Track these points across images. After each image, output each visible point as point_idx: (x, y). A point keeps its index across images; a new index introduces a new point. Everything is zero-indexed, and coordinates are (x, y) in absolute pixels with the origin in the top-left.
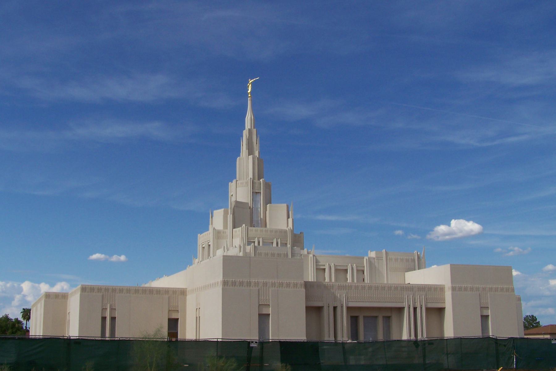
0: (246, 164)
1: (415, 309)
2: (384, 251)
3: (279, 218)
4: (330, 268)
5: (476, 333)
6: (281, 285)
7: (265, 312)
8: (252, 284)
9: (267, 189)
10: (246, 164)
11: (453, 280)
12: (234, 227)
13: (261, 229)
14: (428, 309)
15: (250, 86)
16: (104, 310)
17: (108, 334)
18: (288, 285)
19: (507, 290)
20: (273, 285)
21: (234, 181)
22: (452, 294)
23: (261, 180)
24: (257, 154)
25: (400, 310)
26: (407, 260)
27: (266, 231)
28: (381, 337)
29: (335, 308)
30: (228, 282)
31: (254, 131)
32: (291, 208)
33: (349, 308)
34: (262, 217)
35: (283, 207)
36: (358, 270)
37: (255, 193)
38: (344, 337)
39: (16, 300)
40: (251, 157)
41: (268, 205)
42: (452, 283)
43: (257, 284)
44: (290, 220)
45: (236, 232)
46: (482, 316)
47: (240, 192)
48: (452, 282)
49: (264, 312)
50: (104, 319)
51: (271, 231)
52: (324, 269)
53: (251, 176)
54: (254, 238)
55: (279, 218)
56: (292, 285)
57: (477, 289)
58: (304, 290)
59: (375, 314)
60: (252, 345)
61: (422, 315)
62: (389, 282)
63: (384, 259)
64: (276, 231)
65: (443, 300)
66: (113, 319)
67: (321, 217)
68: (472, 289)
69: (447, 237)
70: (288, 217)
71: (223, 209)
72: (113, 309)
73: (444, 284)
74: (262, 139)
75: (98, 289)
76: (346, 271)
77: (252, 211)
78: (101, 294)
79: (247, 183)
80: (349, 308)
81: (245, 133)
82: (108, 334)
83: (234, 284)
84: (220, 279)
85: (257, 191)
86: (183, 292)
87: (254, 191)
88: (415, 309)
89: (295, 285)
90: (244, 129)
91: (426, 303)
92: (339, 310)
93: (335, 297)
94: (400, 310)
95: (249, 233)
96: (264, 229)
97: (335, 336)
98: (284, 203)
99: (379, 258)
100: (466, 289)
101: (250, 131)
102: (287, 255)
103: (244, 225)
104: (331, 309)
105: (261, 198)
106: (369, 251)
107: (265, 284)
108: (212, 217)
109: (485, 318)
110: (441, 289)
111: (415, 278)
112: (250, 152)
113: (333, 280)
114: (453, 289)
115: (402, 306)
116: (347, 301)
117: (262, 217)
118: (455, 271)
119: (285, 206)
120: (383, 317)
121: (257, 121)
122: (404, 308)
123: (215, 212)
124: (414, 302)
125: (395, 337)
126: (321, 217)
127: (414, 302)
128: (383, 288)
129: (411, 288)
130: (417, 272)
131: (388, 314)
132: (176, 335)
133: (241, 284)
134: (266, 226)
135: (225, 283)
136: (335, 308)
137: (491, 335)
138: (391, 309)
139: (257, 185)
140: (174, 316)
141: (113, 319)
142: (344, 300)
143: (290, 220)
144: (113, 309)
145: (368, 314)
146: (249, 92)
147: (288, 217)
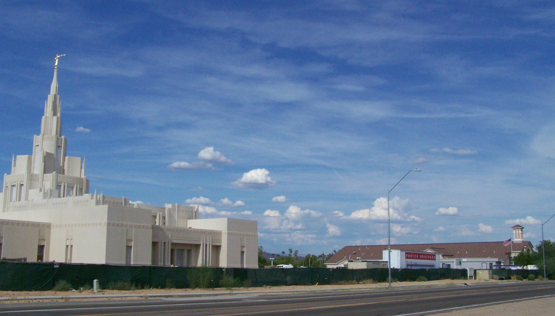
0: (50, 122)
1: (206, 245)
2: (176, 204)
6: (139, 227)
9: (67, 143)
10: (50, 122)
11: (229, 228)
12: (44, 173)
14: (213, 246)
15: (57, 60)
20: (135, 226)
21: (41, 135)
23: (63, 137)
24: (59, 115)
25: (198, 246)
29: (165, 243)
31: (58, 97)
34: (61, 165)
37: (58, 147)
38: (168, 264)
39: (447, 261)
40: (55, 118)
41: (67, 157)
43: (126, 226)
47: (44, 142)
48: (228, 229)
58: (151, 231)
59: (182, 248)
60: (55, 267)
61: (210, 249)
63: (177, 210)
65: (220, 241)
73: (221, 230)
79: (52, 138)
80: (173, 244)
81: (50, 98)
83: (114, 225)
84: (105, 220)
86: (49, 226)
88: (206, 245)
90: (49, 93)
91: (212, 242)
92: (167, 244)
94: (198, 246)
96: (62, 175)
97: (164, 263)
99: (173, 208)
102: (121, 203)
104: (163, 244)
107: (131, 226)
108: (15, 161)
111: (194, 224)
112: (55, 114)
114: (228, 234)
117: (61, 165)
118: (231, 223)
119: (79, 159)
120: (178, 250)
121: (60, 90)
122: (200, 245)
123: (18, 156)
125: (193, 265)
127: (206, 242)
129: (191, 231)
131: (189, 248)
132: (42, 259)
133: (118, 225)
134: (64, 173)
135: (109, 224)
136: (165, 243)
138: (191, 245)
143: (83, 170)
145: (178, 248)
146: (56, 64)
147: (81, 168)
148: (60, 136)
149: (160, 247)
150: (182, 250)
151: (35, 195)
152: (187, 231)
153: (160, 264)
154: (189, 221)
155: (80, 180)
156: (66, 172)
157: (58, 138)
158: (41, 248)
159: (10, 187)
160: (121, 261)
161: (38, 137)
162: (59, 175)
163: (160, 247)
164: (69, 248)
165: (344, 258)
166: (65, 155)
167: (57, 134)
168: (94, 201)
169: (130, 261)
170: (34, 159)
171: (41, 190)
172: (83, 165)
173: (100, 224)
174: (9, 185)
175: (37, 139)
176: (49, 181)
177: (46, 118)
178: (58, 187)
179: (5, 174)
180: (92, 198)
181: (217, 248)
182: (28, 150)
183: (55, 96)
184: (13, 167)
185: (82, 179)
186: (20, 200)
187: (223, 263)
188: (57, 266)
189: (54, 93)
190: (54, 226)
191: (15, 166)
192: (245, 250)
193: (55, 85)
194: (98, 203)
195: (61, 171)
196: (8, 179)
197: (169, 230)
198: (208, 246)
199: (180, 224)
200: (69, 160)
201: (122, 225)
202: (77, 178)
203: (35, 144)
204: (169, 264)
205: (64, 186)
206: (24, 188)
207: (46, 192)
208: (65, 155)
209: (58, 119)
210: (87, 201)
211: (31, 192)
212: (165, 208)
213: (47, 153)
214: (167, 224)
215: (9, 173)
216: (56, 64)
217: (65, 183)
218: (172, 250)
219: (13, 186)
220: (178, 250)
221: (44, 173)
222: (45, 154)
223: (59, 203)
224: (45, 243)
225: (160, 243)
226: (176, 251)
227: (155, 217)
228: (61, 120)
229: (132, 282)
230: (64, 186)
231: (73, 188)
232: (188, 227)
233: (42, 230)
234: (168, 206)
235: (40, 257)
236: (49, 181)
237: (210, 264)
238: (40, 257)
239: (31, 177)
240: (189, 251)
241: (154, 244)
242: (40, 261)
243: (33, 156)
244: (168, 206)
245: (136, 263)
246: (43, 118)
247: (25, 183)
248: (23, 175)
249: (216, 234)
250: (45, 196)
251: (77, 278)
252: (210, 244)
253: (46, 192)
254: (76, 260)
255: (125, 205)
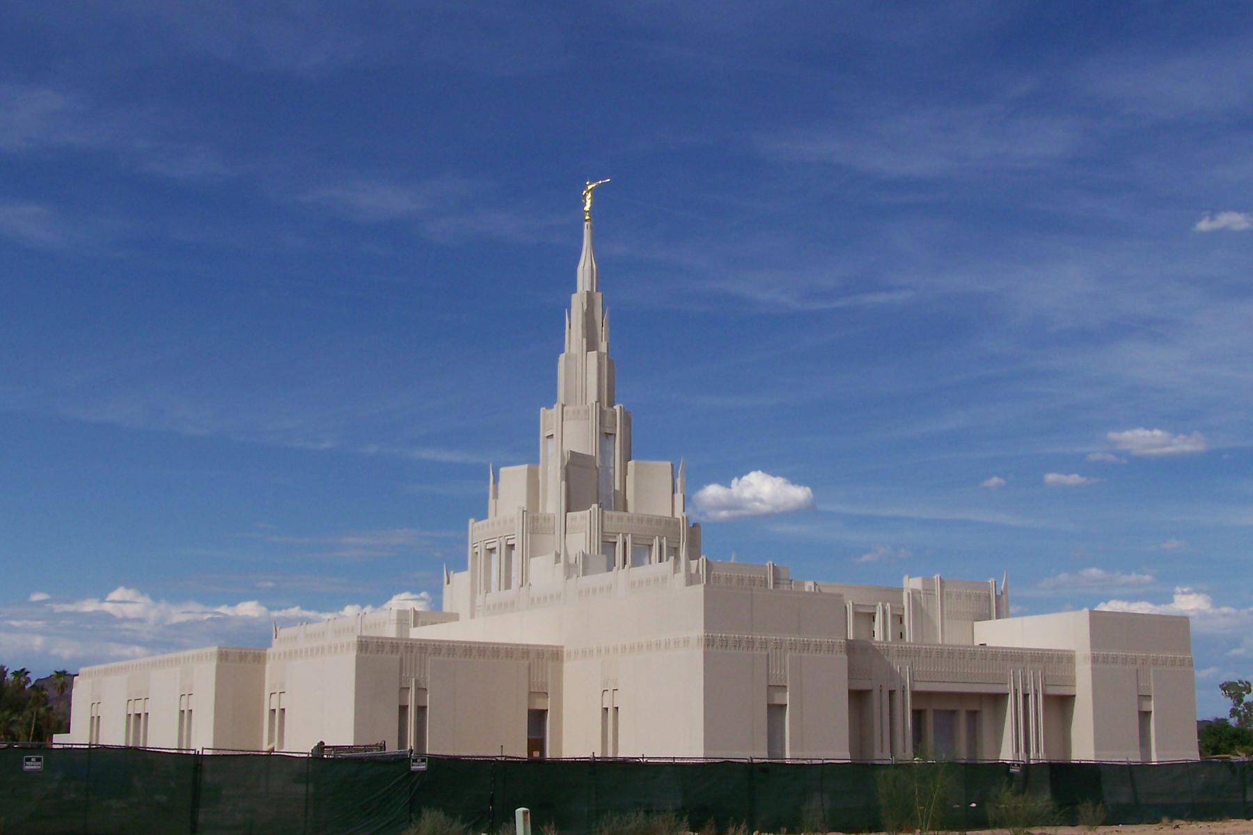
0: (580, 367)
1: (1026, 696)
2: (936, 577)
5: (758, 752)
6: (806, 646)
7: (777, 700)
8: (757, 645)
10: (580, 367)
12: (568, 510)
15: (589, 196)
16: (404, 690)
17: (411, 743)
18: (818, 647)
19: (1182, 661)
20: (793, 646)
21: (557, 408)
22: (1093, 669)
23: (617, 407)
24: (603, 347)
25: (998, 700)
26: (978, 597)
27: (630, 519)
28: (962, 754)
29: (891, 693)
33: (916, 695)
34: (617, 488)
36: (893, 616)
37: (606, 437)
38: (906, 753)
41: (631, 464)
42: (1092, 647)
43: (764, 644)
45: (573, 519)
46: (770, 706)
47: (568, 428)
48: (1094, 644)
49: (777, 702)
50: (403, 709)
51: (640, 520)
53: (592, 396)
54: (615, 535)
57: (1134, 661)
61: (1037, 708)
62: (946, 642)
64: (650, 520)
66: (421, 710)
67: (426, 454)
68: (1125, 660)
69: (724, 514)
71: (526, 466)
72: (421, 691)
73: (1072, 648)
74: (620, 320)
75: (449, 649)
77: (603, 474)
78: (398, 657)
79: (587, 412)
80: (916, 695)
82: (411, 743)
83: (725, 643)
84: (699, 631)
85: (608, 431)
86: (556, 655)
88: (1026, 696)
89: (831, 648)
91: (1045, 685)
93: (892, 671)
94: (998, 700)
95: (606, 522)
96: (623, 514)
97: (1027, 751)
99: (928, 591)
103: (595, 506)
106: (906, 577)
107: (779, 645)
108: (496, 481)
109: (776, 711)
110: (1064, 659)
111: (996, 634)
112: (591, 345)
114: (1095, 659)
115: (865, 688)
116: (913, 681)
117: (617, 488)
118: (1099, 622)
120: (935, 711)
123: (502, 470)
124: (1025, 685)
125: (986, 756)
126: (426, 454)
127: (1025, 685)
128: (940, 653)
130: (995, 623)
131: (975, 707)
132: (542, 749)
133: (738, 643)
134: (625, 510)
135: (709, 642)
136: (891, 693)
137: (788, 755)
139: (608, 418)
140: (539, 706)
141: (421, 710)
142: (912, 677)
144: (421, 691)
146: (587, 208)
148: (611, 404)
149: (878, 704)
150: (953, 712)
151: (543, 572)
152: (973, 655)
153: (881, 755)
154: (978, 626)
155: (672, 523)
156: (631, 508)
157: (602, 412)
158: (537, 719)
159: (482, 556)
160: (1130, 755)
161: (549, 412)
162: (606, 512)
163: (876, 704)
164: (609, 714)
165: (418, 592)
166: (627, 457)
167: (599, 400)
168: (681, 576)
169: (261, 742)
170: (546, 474)
171: (558, 556)
172: (678, 481)
173: (686, 641)
174: (481, 549)
175: (549, 418)
176: (580, 531)
177: (566, 358)
178: (608, 546)
179: (471, 521)
180: (676, 571)
181: (1062, 704)
182: (528, 452)
183: (589, 294)
184: (491, 502)
185: (677, 523)
186: (508, 586)
187: (1083, 750)
188: (423, 767)
189: (588, 288)
190: (569, 654)
191: (496, 496)
192: (1152, 706)
193: (588, 265)
194: (691, 580)
195: (621, 503)
196: (479, 532)
197: (905, 653)
198: (1031, 699)
199: (946, 635)
200: (637, 473)
201: (751, 643)
202: (659, 520)
203: (543, 433)
204: (887, 755)
205: (625, 544)
206: (516, 554)
207: (572, 561)
208: (627, 457)
209: (599, 358)
210: (665, 579)
211: (534, 562)
212: (902, 590)
213: (573, 453)
214: (909, 637)
215: (482, 514)
216: (587, 208)
217: (625, 535)
218: (918, 715)
219: (492, 550)
220: (935, 711)
221: (568, 510)
222: (567, 457)
223: (601, 589)
224: (547, 704)
225: (876, 694)
226: (930, 721)
227: (872, 617)
228: (610, 362)
229: (680, 812)
230: (625, 544)
231: (650, 546)
232: (977, 643)
233: (540, 664)
234: (913, 583)
235: (536, 742)
236: (580, 531)
237: (1038, 754)
238: (536, 742)
239: (533, 521)
240: (973, 715)
241: (858, 697)
242: (536, 754)
243: (540, 467)
244: (913, 583)
245: (798, 754)
246: (562, 357)
247: (517, 542)
248: (512, 520)
249: (1054, 662)
250: (569, 570)
251: (492, 803)
252: (1037, 689)
253: (572, 561)
254: (628, 749)
255: (775, 584)
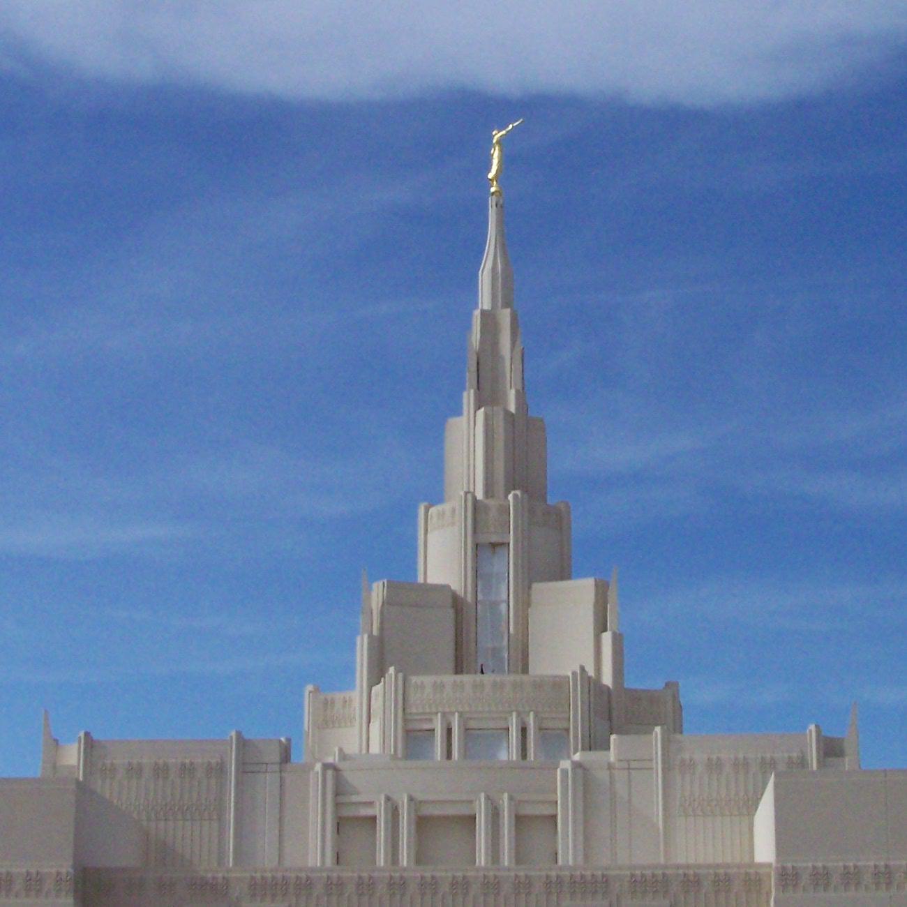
3: (569, 634)
4: (495, 814)
9: (537, 526)
13: (498, 678)
30: (797, 875)
32: (613, 595)
35: (582, 590)
44: (607, 638)
52: (373, 819)
55: (569, 634)
56: (805, 879)
70: (601, 626)
76: (470, 821)
85: (494, 539)
87: (484, 539)
96: (519, 678)
98: (590, 576)
100: (851, 877)
101: (489, 319)
105: (508, 565)
113: (506, 860)
143: (607, 638)
146: (490, 176)
